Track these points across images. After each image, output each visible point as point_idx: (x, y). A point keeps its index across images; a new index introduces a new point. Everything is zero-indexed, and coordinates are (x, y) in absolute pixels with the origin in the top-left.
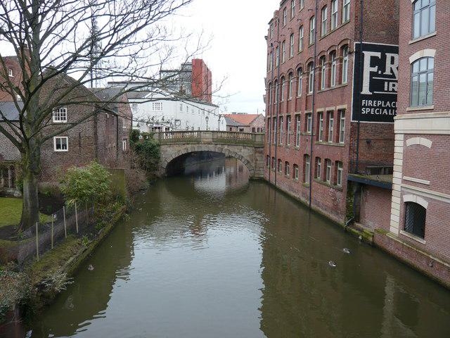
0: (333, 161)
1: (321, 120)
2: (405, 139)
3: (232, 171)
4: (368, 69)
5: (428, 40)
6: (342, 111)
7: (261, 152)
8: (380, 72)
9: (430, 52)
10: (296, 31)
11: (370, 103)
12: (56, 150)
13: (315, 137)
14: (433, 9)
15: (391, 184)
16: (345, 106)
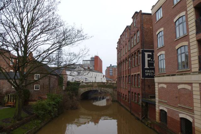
0: (137, 94)
1: (136, 78)
2: (158, 85)
3: (109, 98)
4: (147, 59)
5: (182, 39)
6: (138, 74)
7: (116, 90)
8: (151, 60)
9: (163, 52)
10: (125, 46)
11: (149, 71)
12: (35, 90)
13: (131, 85)
14: (163, 37)
15: (155, 102)
16: (139, 73)
